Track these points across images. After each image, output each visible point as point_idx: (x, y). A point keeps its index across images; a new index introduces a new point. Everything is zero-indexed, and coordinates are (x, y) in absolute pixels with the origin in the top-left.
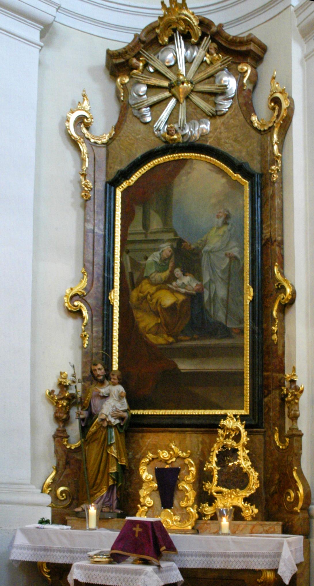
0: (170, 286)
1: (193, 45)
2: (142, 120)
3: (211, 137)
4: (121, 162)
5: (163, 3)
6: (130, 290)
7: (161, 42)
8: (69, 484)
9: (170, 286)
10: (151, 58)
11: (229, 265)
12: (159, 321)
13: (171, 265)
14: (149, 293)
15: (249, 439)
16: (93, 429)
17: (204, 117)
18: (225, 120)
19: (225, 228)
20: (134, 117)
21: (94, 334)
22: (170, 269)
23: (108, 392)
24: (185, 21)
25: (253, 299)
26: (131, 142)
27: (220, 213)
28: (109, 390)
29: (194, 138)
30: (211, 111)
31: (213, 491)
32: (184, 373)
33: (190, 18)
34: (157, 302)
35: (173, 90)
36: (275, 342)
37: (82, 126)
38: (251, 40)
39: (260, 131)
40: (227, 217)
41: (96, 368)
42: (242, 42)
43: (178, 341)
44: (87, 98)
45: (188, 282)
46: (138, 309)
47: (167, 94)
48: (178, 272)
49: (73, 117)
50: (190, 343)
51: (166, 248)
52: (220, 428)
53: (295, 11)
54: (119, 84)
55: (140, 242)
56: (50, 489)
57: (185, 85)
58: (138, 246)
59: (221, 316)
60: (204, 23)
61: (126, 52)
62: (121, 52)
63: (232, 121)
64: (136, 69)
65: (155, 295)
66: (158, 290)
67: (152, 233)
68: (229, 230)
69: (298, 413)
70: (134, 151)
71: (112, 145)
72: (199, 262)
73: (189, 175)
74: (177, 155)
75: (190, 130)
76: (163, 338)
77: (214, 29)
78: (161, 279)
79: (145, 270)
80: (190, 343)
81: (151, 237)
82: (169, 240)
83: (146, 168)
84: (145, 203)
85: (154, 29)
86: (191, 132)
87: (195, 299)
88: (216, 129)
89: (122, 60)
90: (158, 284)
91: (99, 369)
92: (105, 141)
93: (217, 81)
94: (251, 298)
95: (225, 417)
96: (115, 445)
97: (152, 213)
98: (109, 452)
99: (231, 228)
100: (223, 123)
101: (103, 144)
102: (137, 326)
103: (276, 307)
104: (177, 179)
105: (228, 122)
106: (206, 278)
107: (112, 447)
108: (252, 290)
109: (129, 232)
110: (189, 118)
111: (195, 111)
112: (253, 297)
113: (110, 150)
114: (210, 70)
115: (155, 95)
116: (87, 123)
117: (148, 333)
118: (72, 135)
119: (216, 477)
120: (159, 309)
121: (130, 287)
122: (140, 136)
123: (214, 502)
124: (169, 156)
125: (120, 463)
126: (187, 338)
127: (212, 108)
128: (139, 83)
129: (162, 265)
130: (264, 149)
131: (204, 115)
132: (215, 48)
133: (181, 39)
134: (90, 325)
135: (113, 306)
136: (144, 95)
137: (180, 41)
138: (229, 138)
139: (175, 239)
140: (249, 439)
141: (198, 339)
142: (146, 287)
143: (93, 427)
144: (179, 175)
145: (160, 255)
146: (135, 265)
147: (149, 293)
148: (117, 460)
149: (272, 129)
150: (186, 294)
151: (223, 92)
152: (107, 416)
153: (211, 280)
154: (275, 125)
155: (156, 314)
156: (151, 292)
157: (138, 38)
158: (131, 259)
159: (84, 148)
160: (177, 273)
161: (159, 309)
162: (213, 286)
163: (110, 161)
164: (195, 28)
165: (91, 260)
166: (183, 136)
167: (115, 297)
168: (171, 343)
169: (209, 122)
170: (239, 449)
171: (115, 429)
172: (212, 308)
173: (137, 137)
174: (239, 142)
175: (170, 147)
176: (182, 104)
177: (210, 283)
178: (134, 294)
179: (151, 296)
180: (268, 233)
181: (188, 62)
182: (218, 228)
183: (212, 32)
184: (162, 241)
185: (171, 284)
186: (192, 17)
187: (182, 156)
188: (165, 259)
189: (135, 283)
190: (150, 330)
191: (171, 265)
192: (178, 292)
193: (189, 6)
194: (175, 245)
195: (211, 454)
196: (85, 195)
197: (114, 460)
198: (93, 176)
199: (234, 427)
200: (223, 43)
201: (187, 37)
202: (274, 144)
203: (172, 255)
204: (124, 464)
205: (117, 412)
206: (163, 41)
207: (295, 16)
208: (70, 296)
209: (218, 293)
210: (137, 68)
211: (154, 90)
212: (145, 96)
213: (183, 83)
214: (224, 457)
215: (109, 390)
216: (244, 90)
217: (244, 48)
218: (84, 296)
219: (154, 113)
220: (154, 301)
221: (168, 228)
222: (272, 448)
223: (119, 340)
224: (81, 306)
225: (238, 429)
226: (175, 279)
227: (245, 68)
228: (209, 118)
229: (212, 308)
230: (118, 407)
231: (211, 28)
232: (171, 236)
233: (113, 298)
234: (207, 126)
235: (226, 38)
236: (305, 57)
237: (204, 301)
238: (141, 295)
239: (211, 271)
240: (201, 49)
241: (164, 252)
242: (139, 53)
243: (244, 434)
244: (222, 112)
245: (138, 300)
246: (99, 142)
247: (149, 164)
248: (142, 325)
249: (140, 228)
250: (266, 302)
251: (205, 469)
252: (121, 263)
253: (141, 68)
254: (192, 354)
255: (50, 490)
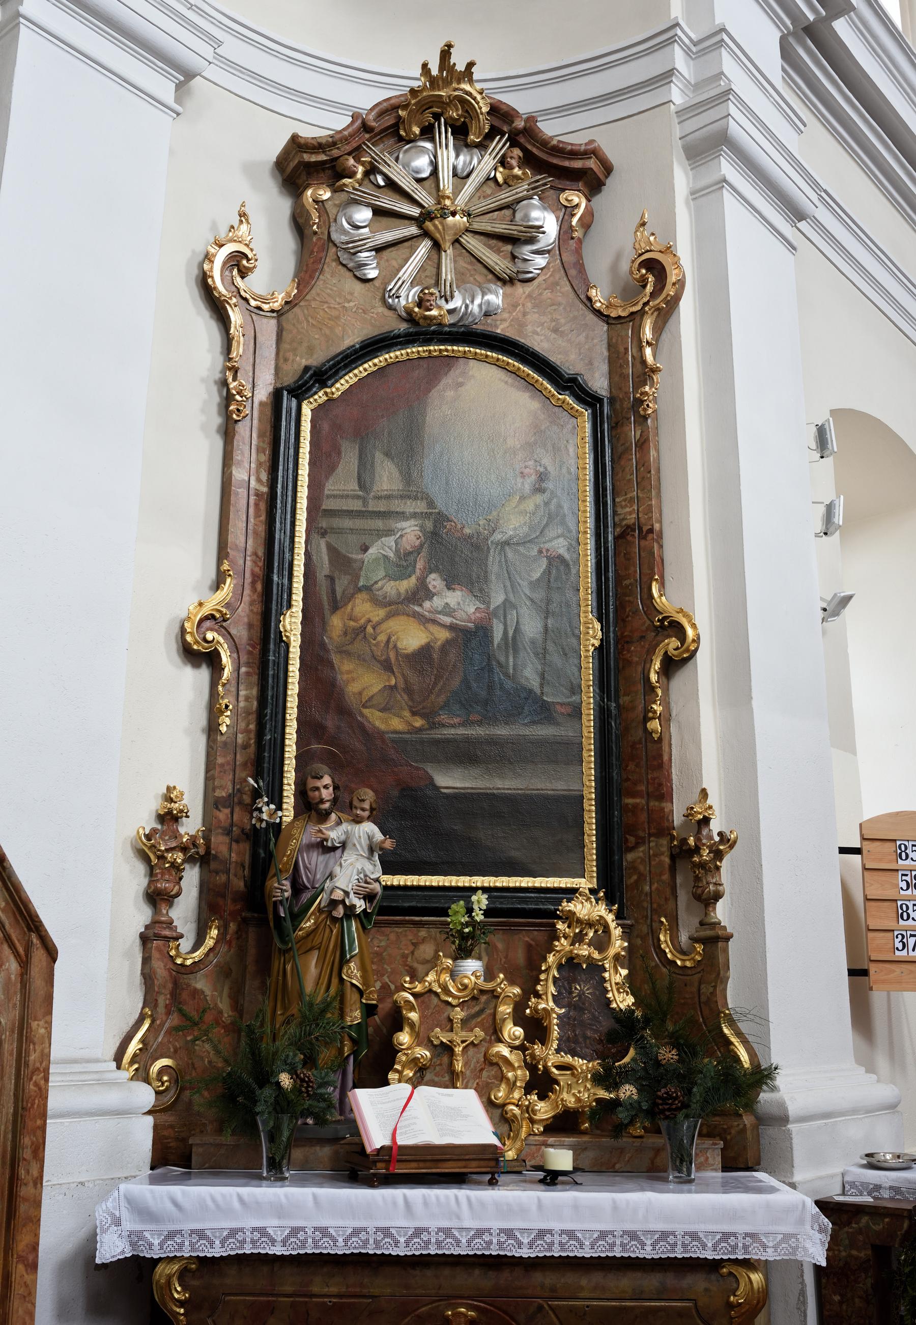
0: (417, 608)
1: (469, 146)
2: (357, 274)
3: (505, 320)
4: (311, 350)
5: (425, 66)
6: (327, 612)
7: (402, 133)
8: (176, 1051)
9: (417, 608)
10: (386, 163)
11: (548, 572)
12: (393, 682)
13: (420, 565)
14: (369, 621)
15: (626, 944)
16: (308, 924)
17: (489, 281)
18: (533, 290)
19: (539, 499)
20: (340, 267)
21: (242, 704)
22: (418, 572)
23: (343, 838)
24: (463, 101)
25: (601, 645)
26: (334, 313)
27: (526, 467)
28: (346, 833)
29: (470, 319)
30: (508, 271)
31: (550, 1064)
32: (447, 796)
33: (475, 99)
34: (388, 641)
35: (428, 225)
36: (656, 736)
37: (235, 272)
38: (593, 152)
39: (608, 316)
40: (542, 477)
41: (319, 784)
42: (574, 154)
43: (433, 726)
44: (247, 220)
45: (459, 604)
46: (343, 652)
47: (413, 230)
48: (435, 581)
49: (221, 255)
50: (461, 731)
51: (408, 530)
52: (559, 918)
53: (676, 113)
54: (311, 200)
55: (350, 514)
56: (136, 1066)
57: (457, 217)
58: (347, 523)
59: (530, 675)
60: (499, 112)
61: (334, 144)
62: (324, 141)
63: (547, 294)
64: (350, 178)
65: (384, 626)
66: (389, 616)
67: (379, 498)
68: (547, 504)
69: (721, 888)
70: (338, 330)
71: (290, 315)
72: (483, 563)
73: (463, 389)
74: (436, 348)
75: (464, 301)
76: (401, 717)
77: (520, 124)
78: (399, 594)
79: (363, 573)
80: (461, 731)
81: (372, 506)
82: (414, 515)
83: (369, 366)
84: (362, 434)
85: (395, 108)
86: (467, 307)
87: (472, 637)
88: (515, 306)
89: (322, 157)
90: (390, 604)
91: (326, 787)
92: (276, 306)
93: (519, 216)
94: (597, 643)
95: (571, 893)
96: (357, 959)
97: (379, 456)
98: (345, 977)
99: (550, 500)
100: (529, 296)
101: (273, 311)
102: (342, 694)
103: (657, 665)
104: (434, 393)
105: (541, 294)
106: (498, 599)
107: (352, 964)
108: (598, 626)
109: (326, 492)
110: (461, 278)
111: (469, 267)
112: (602, 640)
113: (284, 325)
114: (505, 196)
115: (388, 228)
116: (244, 267)
117: (364, 706)
118: (215, 288)
119: (555, 1032)
120: (392, 655)
121: (326, 606)
122: (352, 304)
123: (553, 1090)
124: (420, 349)
125: (364, 1001)
126: (456, 720)
127: (510, 265)
128: (356, 202)
129: (402, 565)
130: (618, 352)
131: (490, 276)
132: (520, 157)
133: (450, 134)
134: (234, 682)
135: (288, 646)
136: (365, 227)
137: (446, 137)
138: (542, 324)
139: (431, 513)
140: (626, 944)
141: (480, 723)
142: (362, 608)
143: (309, 920)
144: (441, 386)
145: (396, 543)
146: (339, 559)
147: (369, 621)
148: (361, 993)
149: (638, 318)
150: (452, 628)
151: (530, 235)
152: (347, 893)
153: (506, 601)
154: (647, 309)
155: (387, 666)
156: (375, 619)
157: (359, 122)
158: (330, 547)
159: (236, 317)
160: (434, 583)
161: (392, 655)
162: (512, 616)
163: (285, 346)
164: (481, 116)
165: (243, 545)
166: (450, 312)
167: (292, 624)
168: (420, 730)
169: (501, 291)
170: (607, 966)
171: (356, 922)
172: (511, 660)
173: (346, 305)
174: (562, 334)
175: (419, 329)
176: (445, 251)
177: (505, 607)
178: (336, 622)
179: (374, 628)
180: (630, 513)
181: (460, 177)
182: (523, 498)
183: (516, 129)
184: (402, 516)
185: (421, 605)
186: (479, 97)
187: (447, 350)
188: (408, 554)
189: (339, 598)
190: (371, 698)
191: (420, 565)
192: (434, 622)
193: (475, 77)
194: (429, 525)
195: (543, 977)
196: (238, 410)
197: (356, 996)
198: (251, 374)
199: (595, 916)
200: (535, 151)
201: (460, 131)
202: (644, 344)
203: (422, 546)
204: (374, 1002)
205: (366, 882)
206: (408, 131)
207: (676, 121)
208: (198, 619)
209: (522, 627)
210: (352, 175)
211: (385, 221)
212: (366, 230)
213: (454, 214)
214: (570, 984)
215: (346, 833)
216: (572, 238)
217: (578, 164)
218: (225, 620)
219: (382, 262)
220: (382, 638)
221: (412, 488)
222: (653, 964)
223: (298, 720)
224: (218, 642)
225: (602, 921)
226: (430, 595)
227: (576, 200)
228: (499, 283)
229: (511, 660)
230: (368, 873)
231: (513, 122)
232: (421, 506)
233: (288, 627)
234: (497, 296)
235: (544, 144)
236: (692, 193)
237: (492, 643)
238: (352, 623)
239: (508, 584)
240: (487, 157)
241: (404, 539)
242: (358, 148)
243: (616, 932)
244: (530, 275)
245: (345, 634)
246: (266, 307)
247: (376, 361)
248: (353, 688)
249: (352, 486)
250: (629, 651)
251: (528, 1011)
252: (307, 553)
253: (359, 176)
254: (464, 754)
255: (136, 1070)
